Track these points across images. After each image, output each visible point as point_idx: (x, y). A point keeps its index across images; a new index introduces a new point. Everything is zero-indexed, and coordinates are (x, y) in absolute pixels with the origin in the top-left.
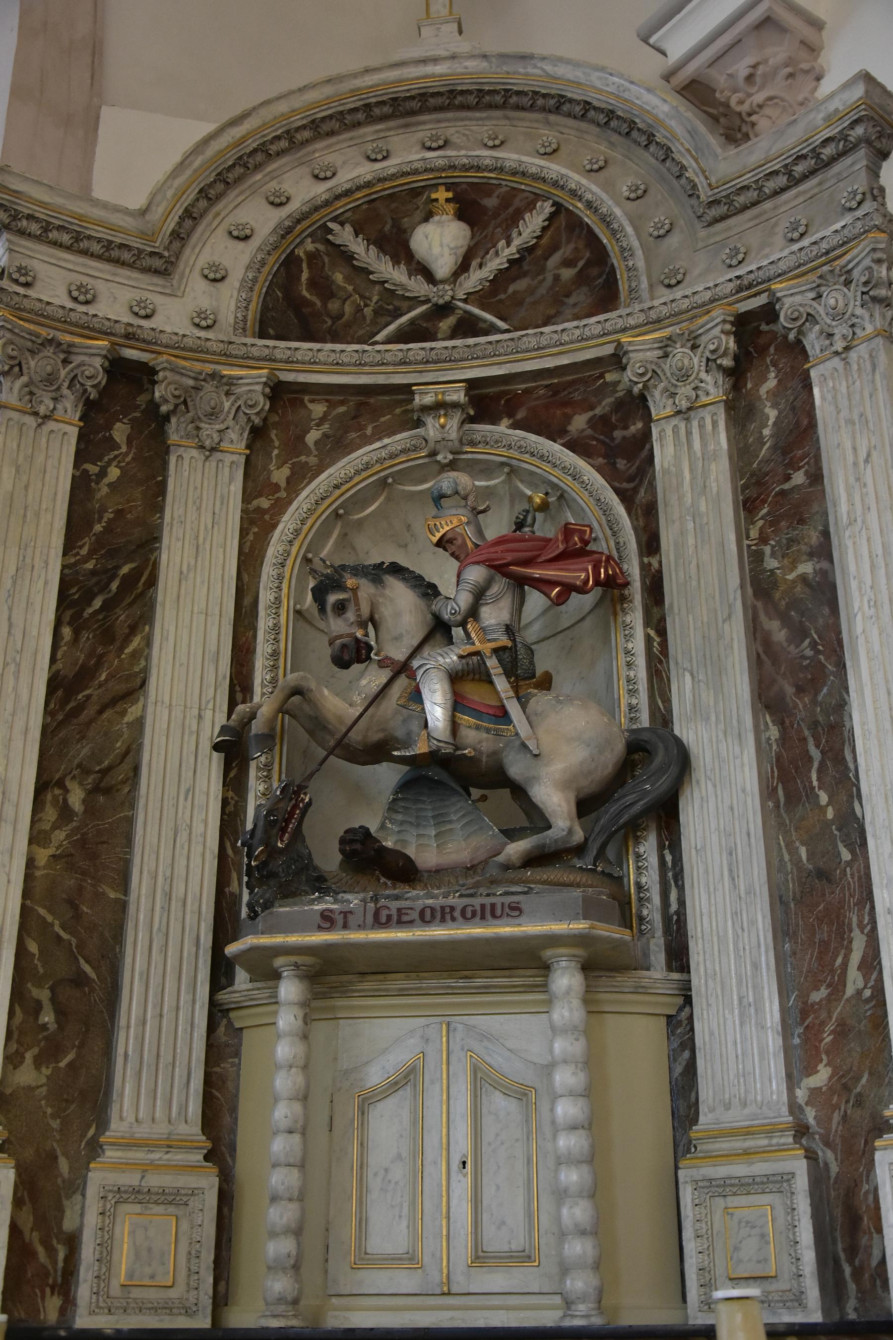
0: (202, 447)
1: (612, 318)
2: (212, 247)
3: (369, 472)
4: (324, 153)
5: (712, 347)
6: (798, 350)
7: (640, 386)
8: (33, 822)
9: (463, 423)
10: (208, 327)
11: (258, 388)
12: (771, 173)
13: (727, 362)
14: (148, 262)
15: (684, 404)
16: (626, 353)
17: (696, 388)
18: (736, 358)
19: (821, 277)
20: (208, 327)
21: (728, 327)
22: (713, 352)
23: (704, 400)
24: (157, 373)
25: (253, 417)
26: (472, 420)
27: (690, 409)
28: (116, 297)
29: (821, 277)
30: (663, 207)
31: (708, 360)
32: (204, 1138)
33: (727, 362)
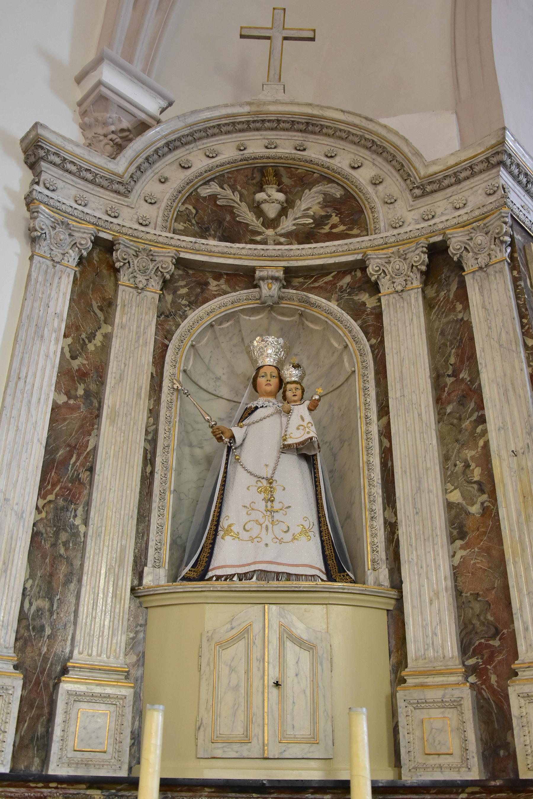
0: (137, 288)
1: (364, 241)
2: (148, 185)
3: (240, 304)
4: (211, 143)
5: (497, 231)
6: (459, 267)
7: (376, 276)
8: (389, 418)
9: (280, 288)
10: (146, 225)
11: (170, 259)
12: (431, 182)
13: (424, 268)
14: (116, 186)
15: (399, 288)
16: (369, 259)
17: (406, 280)
18: (428, 266)
19: (473, 228)
20: (146, 225)
21: (425, 249)
22: (498, 233)
23: (494, 260)
24: (115, 245)
25: (165, 274)
26: (284, 287)
27: (402, 291)
28: (98, 204)
29: (473, 228)
30: (393, 185)
31: (495, 238)
32: (14, 655)
33: (424, 268)
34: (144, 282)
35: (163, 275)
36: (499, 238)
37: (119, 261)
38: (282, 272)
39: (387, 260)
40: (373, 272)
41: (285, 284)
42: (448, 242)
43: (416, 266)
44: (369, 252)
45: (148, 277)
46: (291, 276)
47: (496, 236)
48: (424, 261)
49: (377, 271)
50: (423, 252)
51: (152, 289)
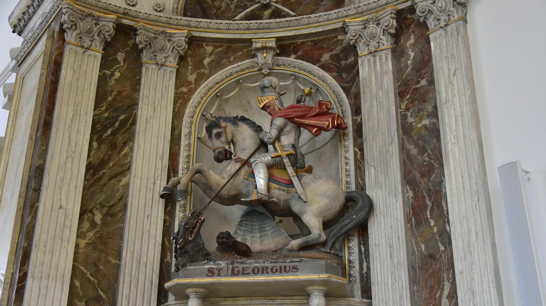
5: (386, 24)
6: (424, 26)
7: (354, 41)
8: (78, 228)
15: (373, 49)
16: (347, 26)
17: (378, 43)
18: (396, 29)
21: (393, 15)
23: (382, 47)
24: (137, 30)
25: (180, 51)
26: (278, 55)
27: (375, 51)
31: (384, 30)
34: (164, 60)
35: (178, 52)
36: (387, 30)
37: (142, 43)
38: (274, 43)
39: (363, 27)
40: (351, 38)
41: (278, 52)
42: (415, 7)
43: (387, 30)
44: (347, 20)
45: (166, 55)
46: (284, 47)
47: (385, 29)
48: (392, 25)
49: (354, 36)
50: (393, 18)
51: (170, 65)
